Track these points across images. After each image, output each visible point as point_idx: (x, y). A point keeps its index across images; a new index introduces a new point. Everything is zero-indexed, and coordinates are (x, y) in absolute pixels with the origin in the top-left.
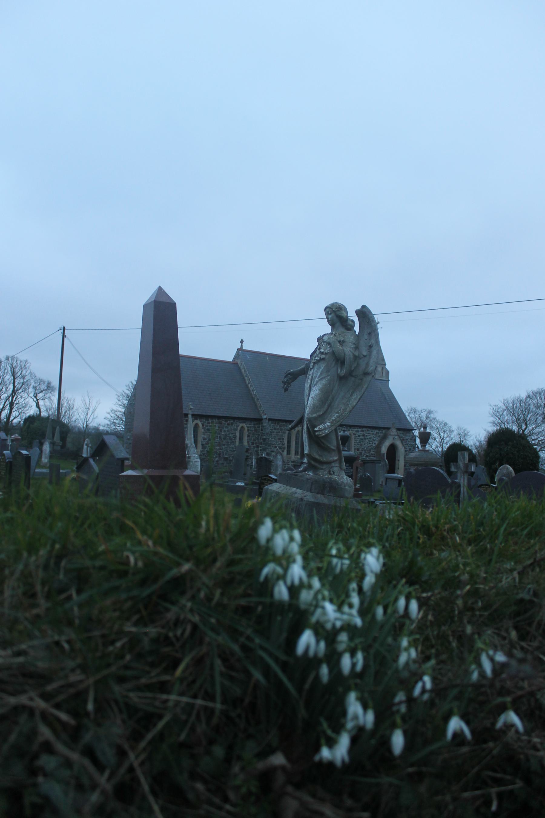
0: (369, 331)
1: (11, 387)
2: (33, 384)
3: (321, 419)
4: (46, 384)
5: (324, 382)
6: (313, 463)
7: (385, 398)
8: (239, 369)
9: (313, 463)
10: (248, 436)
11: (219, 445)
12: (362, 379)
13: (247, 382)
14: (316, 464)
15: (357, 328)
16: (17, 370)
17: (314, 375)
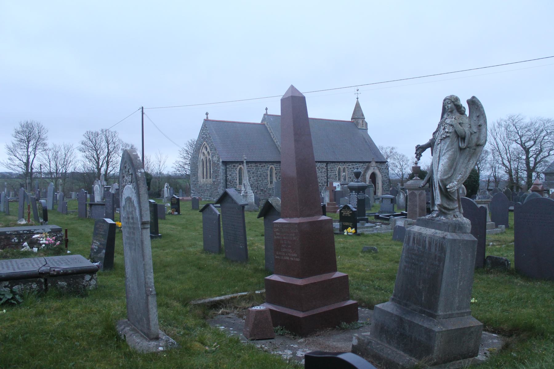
0: (478, 115)
1: (106, 150)
2: (121, 147)
3: (450, 179)
4: (130, 146)
5: (450, 153)
6: (443, 210)
7: (366, 142)
8: (266, 128)
9: (443, 210)
10: (276, 174)
11: (257, 181)
12: (475, 149)
13: (272, 136)
14: (446, 211)
15: (467, 113)
16: (109, 138)
17: (442, 148)
